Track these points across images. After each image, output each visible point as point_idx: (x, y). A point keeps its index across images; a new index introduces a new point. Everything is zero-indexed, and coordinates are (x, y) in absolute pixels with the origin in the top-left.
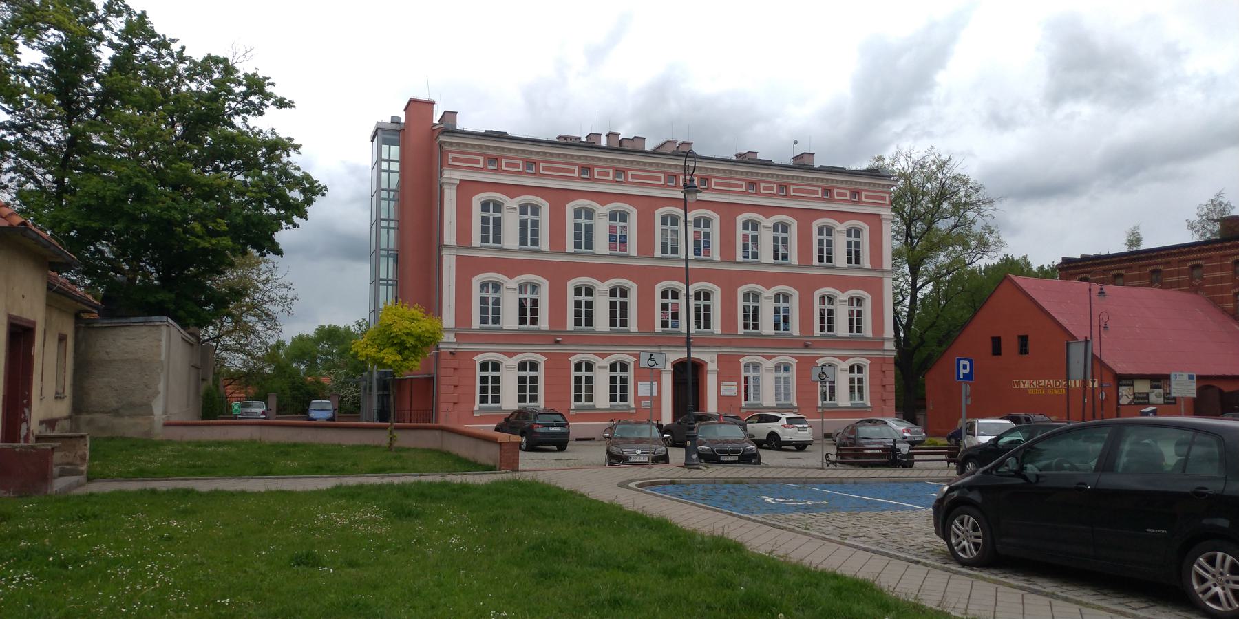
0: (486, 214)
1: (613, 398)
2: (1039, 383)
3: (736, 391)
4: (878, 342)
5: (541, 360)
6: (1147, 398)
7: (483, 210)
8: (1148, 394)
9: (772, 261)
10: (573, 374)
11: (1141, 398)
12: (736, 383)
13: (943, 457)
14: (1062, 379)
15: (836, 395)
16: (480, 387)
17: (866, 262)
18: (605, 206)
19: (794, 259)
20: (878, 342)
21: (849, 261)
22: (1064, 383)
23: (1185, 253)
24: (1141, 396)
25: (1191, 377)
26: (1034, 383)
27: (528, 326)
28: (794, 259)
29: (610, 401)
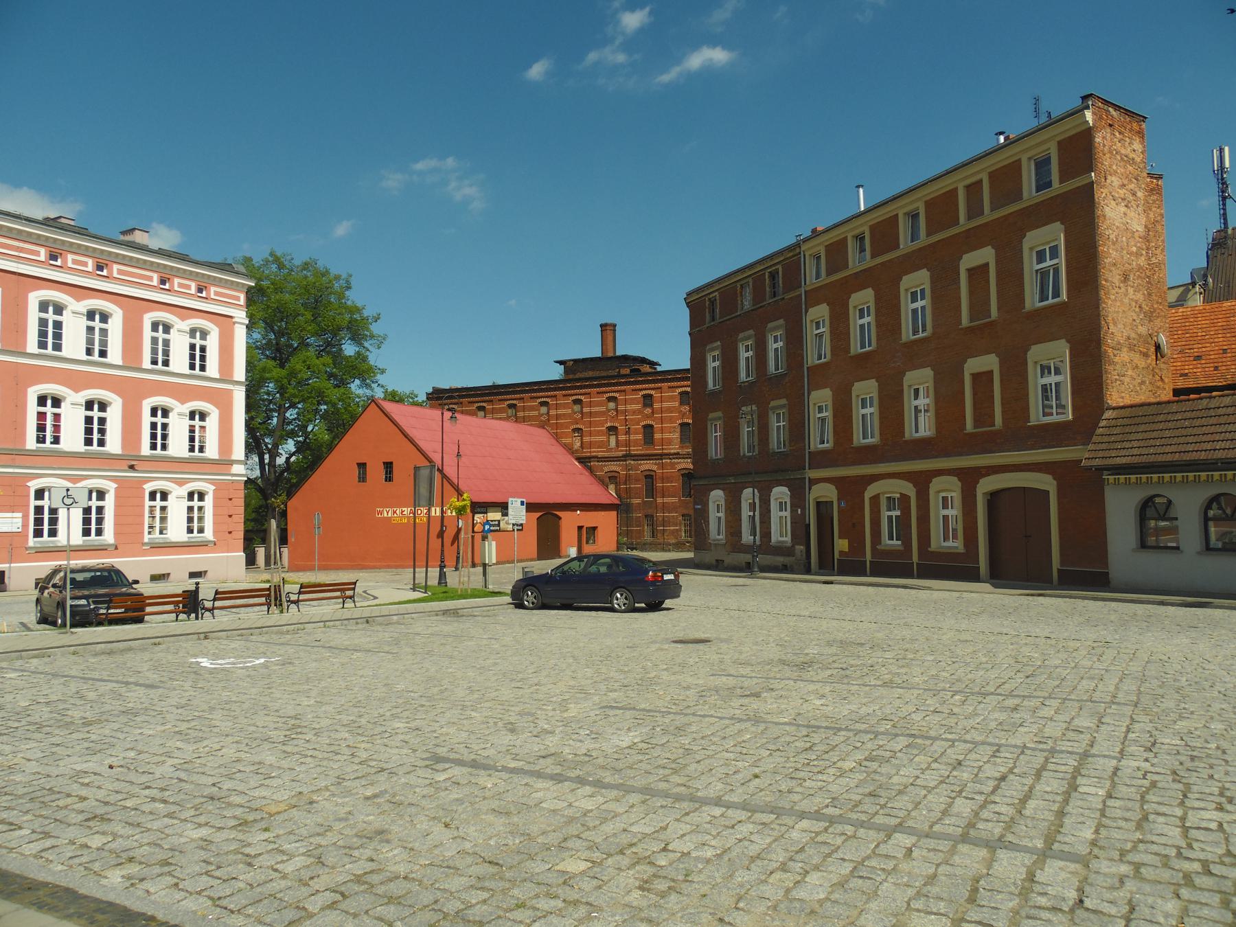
0: (43, 315)
1: (86, 532)
2: (402, 512)
3: (20, 525)
4: (225, 462)
5: (111, 487)
6: (499, 525)
7: (41, 310)
8: (499, 521)
9: (187, 371)
10: (148, 503)
11: (494, 526)
12: (20, 515)
13: (170, 607)
14: (423, 507)
15: (169, 528)
16: (35, 518)
17: (213, 369)
18: (81, 303)
19: (115, 354)
20: (225, 462)
21: (192, 367)
22: (425, 511)
23: (535, 391)
24: (494, 523)
25: (522, 503)
26: (398, 512)
27: (159, 451)
28: (115, 354)
29: (83, 536)
